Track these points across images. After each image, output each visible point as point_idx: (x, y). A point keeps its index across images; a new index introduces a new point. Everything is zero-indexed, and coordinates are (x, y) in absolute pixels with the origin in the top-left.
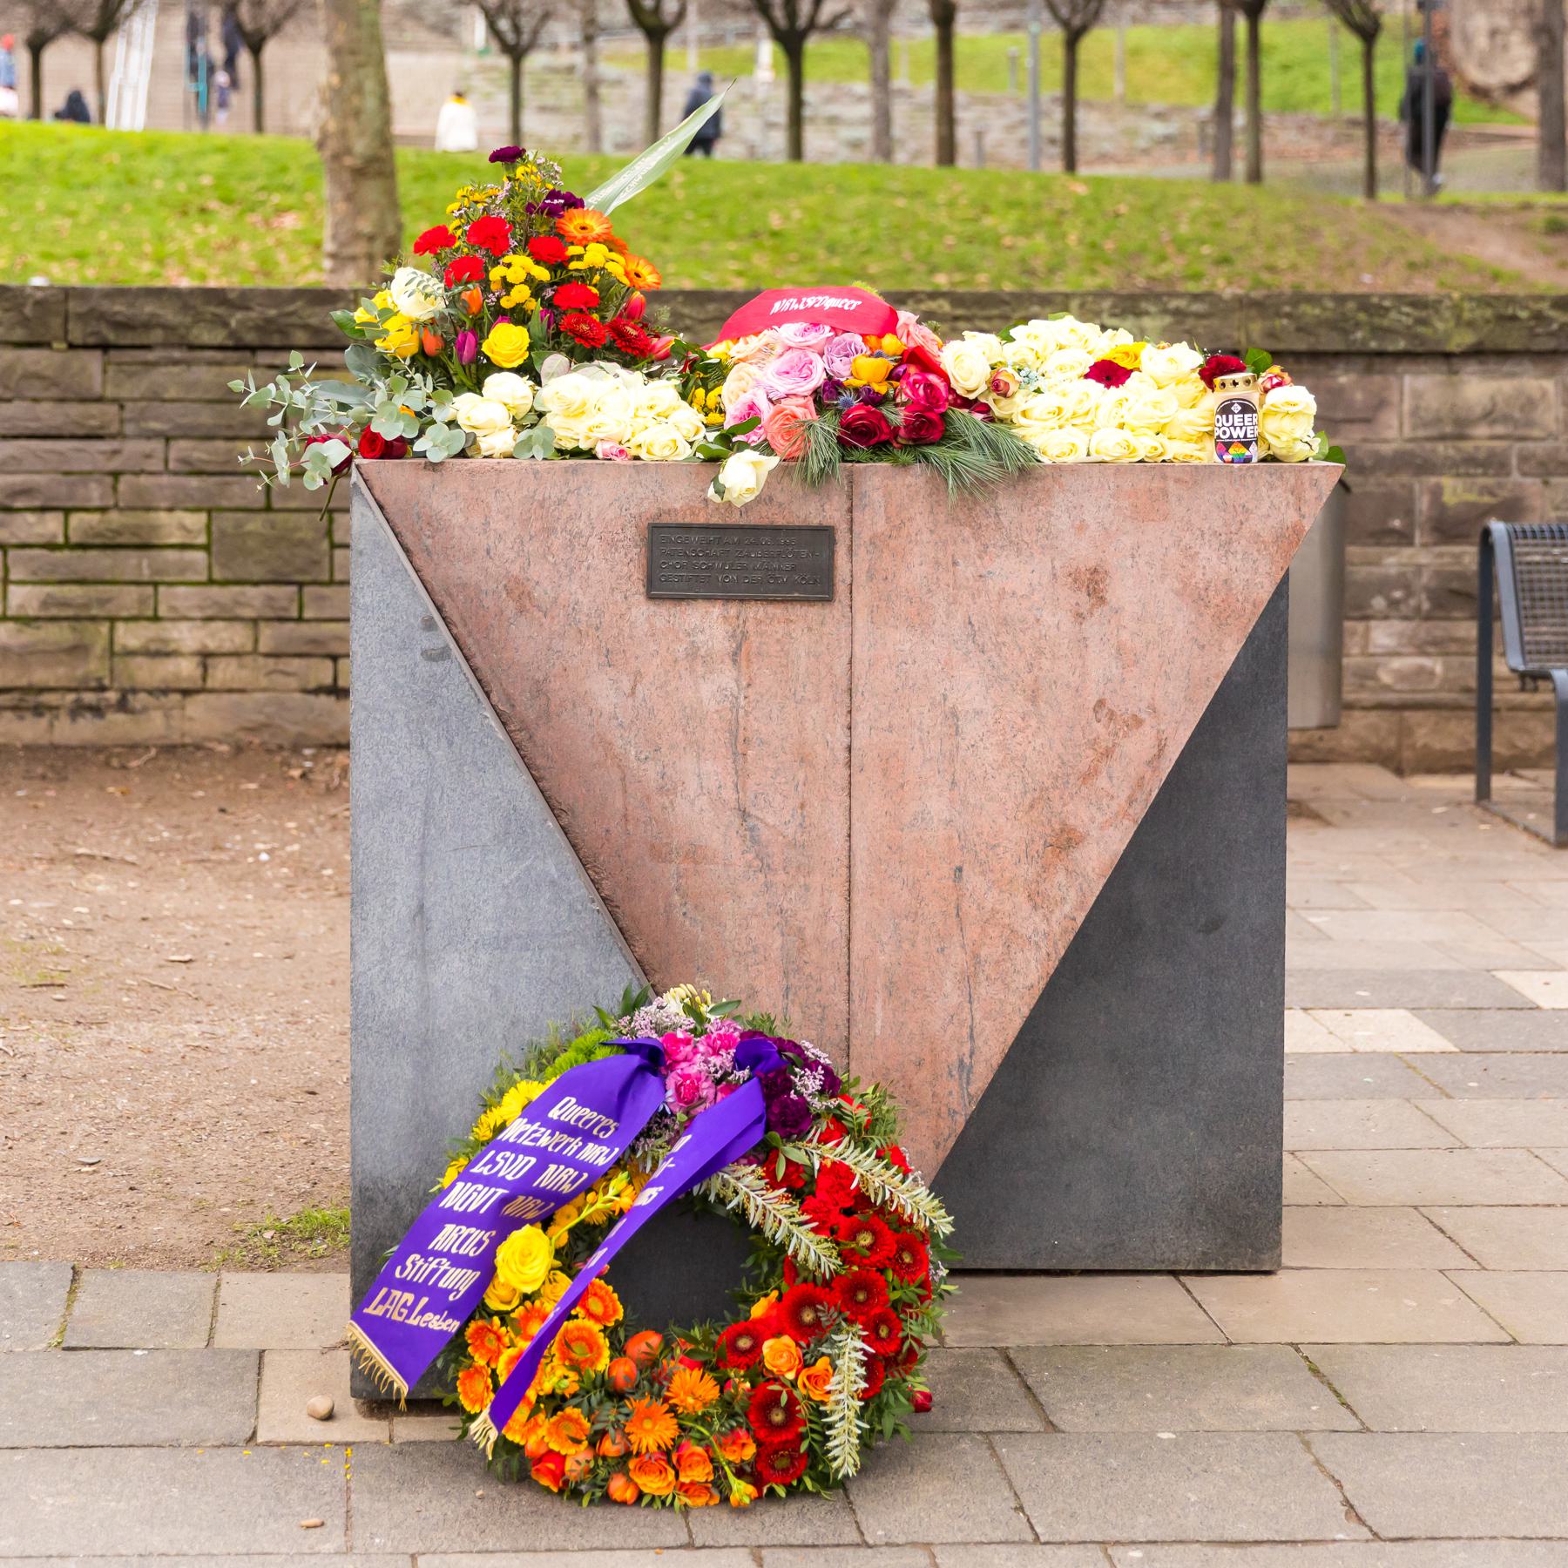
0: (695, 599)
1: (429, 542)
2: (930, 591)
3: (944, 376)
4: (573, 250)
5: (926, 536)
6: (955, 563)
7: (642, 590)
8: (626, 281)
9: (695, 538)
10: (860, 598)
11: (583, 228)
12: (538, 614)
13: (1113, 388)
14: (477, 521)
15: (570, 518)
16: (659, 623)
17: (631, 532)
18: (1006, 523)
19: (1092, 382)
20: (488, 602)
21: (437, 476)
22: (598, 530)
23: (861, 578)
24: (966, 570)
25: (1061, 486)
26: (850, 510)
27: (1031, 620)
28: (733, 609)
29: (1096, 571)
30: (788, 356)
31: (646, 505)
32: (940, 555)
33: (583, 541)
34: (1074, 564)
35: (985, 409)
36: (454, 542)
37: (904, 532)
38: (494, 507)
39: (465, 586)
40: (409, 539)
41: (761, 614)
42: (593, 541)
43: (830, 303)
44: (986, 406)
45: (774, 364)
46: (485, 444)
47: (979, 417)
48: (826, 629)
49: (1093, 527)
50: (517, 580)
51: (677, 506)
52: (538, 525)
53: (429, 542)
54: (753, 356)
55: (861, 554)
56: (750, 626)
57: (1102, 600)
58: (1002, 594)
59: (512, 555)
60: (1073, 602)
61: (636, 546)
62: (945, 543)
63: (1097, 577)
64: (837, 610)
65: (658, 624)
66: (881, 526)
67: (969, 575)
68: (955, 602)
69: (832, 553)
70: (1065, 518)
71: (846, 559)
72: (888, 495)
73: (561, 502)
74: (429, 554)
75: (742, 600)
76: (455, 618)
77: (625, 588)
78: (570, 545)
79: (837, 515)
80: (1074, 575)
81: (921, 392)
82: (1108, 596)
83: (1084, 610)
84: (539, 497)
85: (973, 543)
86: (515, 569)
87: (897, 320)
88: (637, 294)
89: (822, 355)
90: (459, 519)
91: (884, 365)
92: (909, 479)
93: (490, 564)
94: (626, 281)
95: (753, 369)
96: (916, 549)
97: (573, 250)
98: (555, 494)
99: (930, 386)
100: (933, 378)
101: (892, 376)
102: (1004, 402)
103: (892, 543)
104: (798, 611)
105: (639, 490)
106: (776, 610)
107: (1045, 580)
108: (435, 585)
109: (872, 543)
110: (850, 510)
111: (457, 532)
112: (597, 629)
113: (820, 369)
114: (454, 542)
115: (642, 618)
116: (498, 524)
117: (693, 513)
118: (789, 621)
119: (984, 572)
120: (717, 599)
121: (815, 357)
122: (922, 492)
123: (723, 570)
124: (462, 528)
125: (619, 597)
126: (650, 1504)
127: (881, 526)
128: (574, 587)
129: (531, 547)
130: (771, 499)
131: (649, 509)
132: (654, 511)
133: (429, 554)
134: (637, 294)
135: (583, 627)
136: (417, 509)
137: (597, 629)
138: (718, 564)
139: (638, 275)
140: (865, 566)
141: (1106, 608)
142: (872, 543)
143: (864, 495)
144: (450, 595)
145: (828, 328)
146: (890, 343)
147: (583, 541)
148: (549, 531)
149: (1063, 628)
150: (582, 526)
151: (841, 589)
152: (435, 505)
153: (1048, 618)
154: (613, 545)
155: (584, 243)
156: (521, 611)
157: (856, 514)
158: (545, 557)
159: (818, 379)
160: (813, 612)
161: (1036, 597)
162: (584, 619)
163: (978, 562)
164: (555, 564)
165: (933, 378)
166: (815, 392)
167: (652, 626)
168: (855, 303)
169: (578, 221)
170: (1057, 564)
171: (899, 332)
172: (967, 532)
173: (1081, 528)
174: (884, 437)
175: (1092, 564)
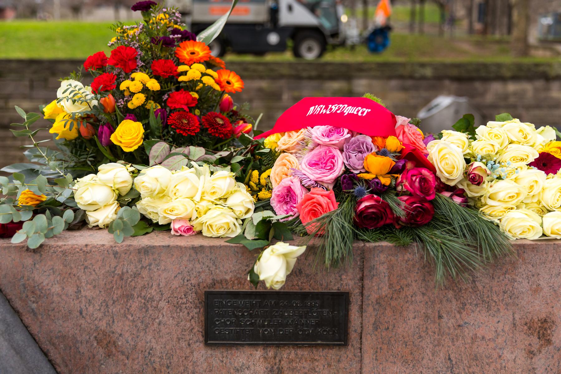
0: (242, 345)
1: (34, 306)
2: (420, 337)
3: (432, 169)
4: (181, 68)
5: (419, 298)
6: (440, 317)
7: (201, 339)
8: (217, 88)
9: (240, 302)
10: (369, 342)
11: (193, 53)
12: (121, 357)
13: (551, 175)
14: (71, 290)
15: (144, 287)
16: (215, 363)
17: (191, 297)
18: (480, 288)
19: (535, 170)
20: (83, 349)
21: (37, 257)
22: (166, 295)
23: (368, 328)
24: (448, 322)
25: (524, 260)
26: (362, 279)
27: (495, 356)
28: (271, 353)
29: (545, 321)
30: (317, 150)
31: (203, 276)
32: (430, 311)
33: (154, 304)
34: (530, 317)
35: (461, 193)
36: (54, 305)
37: (402, 295)
38: (84, 278)
39: (64, 337)
40: (18, 304)
41: (292, 356)
42: (162, 304)
43: (348, 110)
44: (463, 191)
45: (307, 157)
46: (93, 217)
47: (458, 200)
48: (342, 365)
49: (546, 289)
50: (104, 333)
51: (228, 277)
52: (119, 292)
53: (34, 306)
54: (293, 148)
55: (370, 311)
56: (284, 364)
57: (549, 342)
58: (474, 338)
59: (100, 315)
60: (527, 343)
61: (196, 307)
62: (433, 302)
63: (546, 325)
64: (349, 353)
65: (215, 364)
66: (385, 290)
67: (450, 325)
68: (439, 344)
69: (347, 311)
70: (525, 283)
71: (357, 314)
72: (391, 268)
73: (136, 275)
74: (35, 314)
75: (278, 346)
76: (58, 361)
77: (188, 338)
78: (145, 308)
79: (351, 283)
80: (529, 326)
81: (417, 184)
82: (553, 339)
83: (535, 348)
84: (118, 272)
85: (454, 301)
86: (103, 325)
87: (395, 122)
88: (226, 96)
89: (342, 151)
90: (56, 289)
91: (387, 162)
92: (408, 256)
93: (82, 321)
94: (217, 88)
95: (292, 158)
96: (411, 307)
97: (181, 68)
98: (131, 269)
99: (423, 180)
100: (425, 172)
101: (394, 171)
102: (474, 187)
103: (393, 303)
104: (320, 354)
105: (198, 266)
106: (304, 353)
107: (507, 328)
108: (41, 337)
109: (378, 303)
110: (362, 279)
111: (56, 299)
112: (168, 367)
113: (340, 162)
114: (54, 305)
115: (202, 359)
116: (87, 292)
117: (240, 283)
118: (313, 360)
119: (462, 323)
120: (258, 345)
121: (337, 152)
122: (418, 265)
123: (264, 326)
124: (59, 295)
125: (184, 344)
126: (320, 237)
127: (385, 290)
128: (149, 337)
129: (114, 309)
130: (300, 272)
131: (206, 278)
132: (209, 281)
133: (35, 314)
134: (226, 96)
135: (157, 366)
136: (22, 282)
137: (168, 367)
138: (259, 321)
139: (229, 83)
140: (372, 320)
141: (551, 347)
142: (378, 303)
143: (373, 268)
144: (54, 344)
145: (346, 131)
146: (392, 143)
147: (154, 304)
148: (129, 297)
149: (519, 361)
150: (154, 293)
151: (354, 336)
152: (37, 278)
153: (507, 355)
154: (178, 307)
155: (190, 64)
156: (109, 355)
157: (367, 282)
158: (125, 316)
159: (339, 170)
160: (332, 353)
161: (500, 340)
162: (158, 360)
163: (458, 316)
164: (133, 321)
165: (425, 172)
166: (337, 180)
167: (209, 364)
168: (366, 111)
169: (190, 49)
170: (517, 316)
171: (397, 132)
172: (450, 294)
173: (537, 290)
174: (388, 221)
175: (543, 316)
